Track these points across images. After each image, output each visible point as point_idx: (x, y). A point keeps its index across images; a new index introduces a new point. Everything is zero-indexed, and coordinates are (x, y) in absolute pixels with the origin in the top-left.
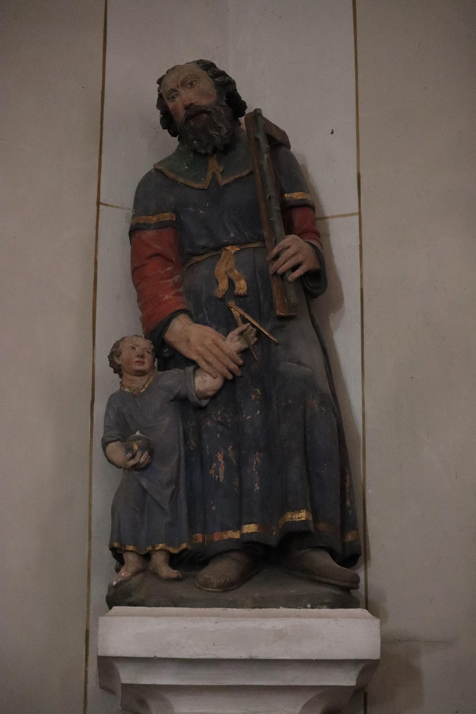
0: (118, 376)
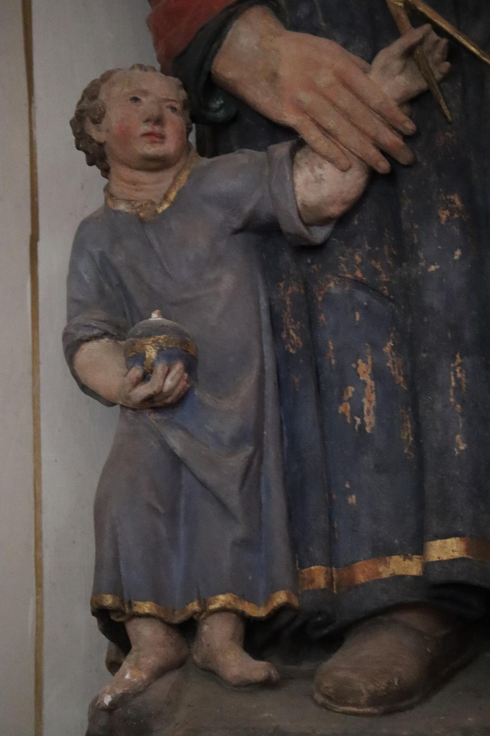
0: (98, 171)
